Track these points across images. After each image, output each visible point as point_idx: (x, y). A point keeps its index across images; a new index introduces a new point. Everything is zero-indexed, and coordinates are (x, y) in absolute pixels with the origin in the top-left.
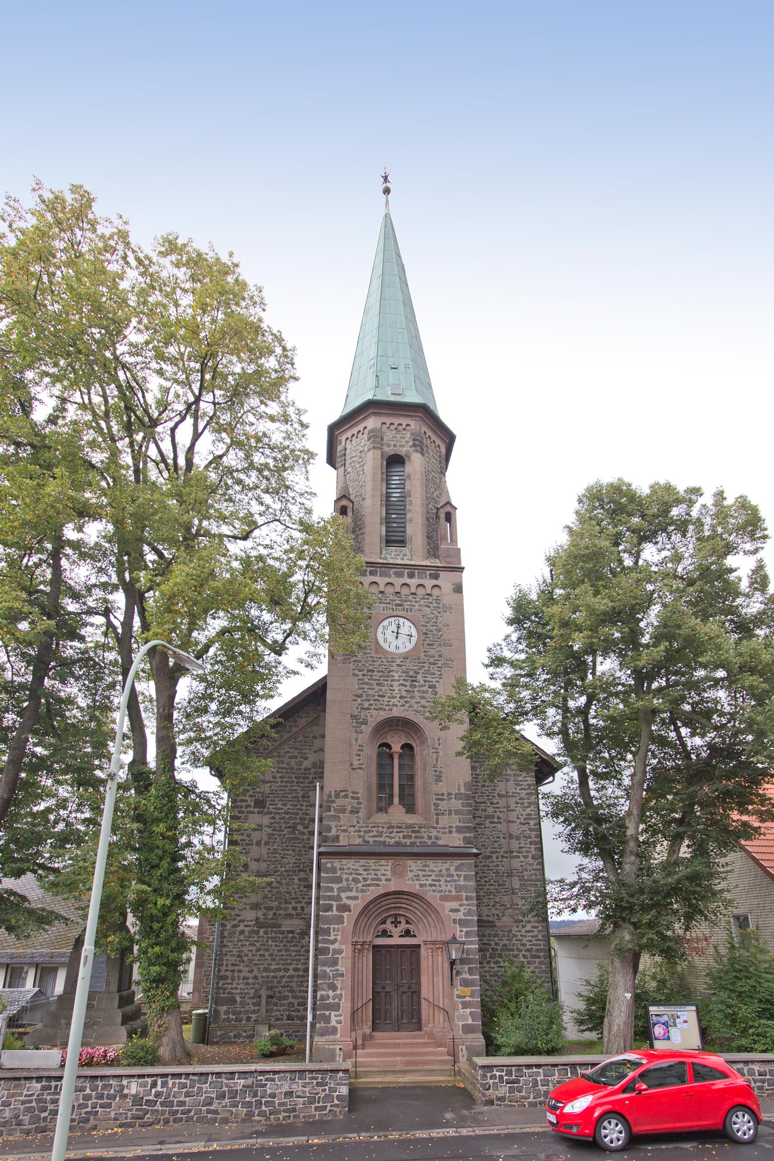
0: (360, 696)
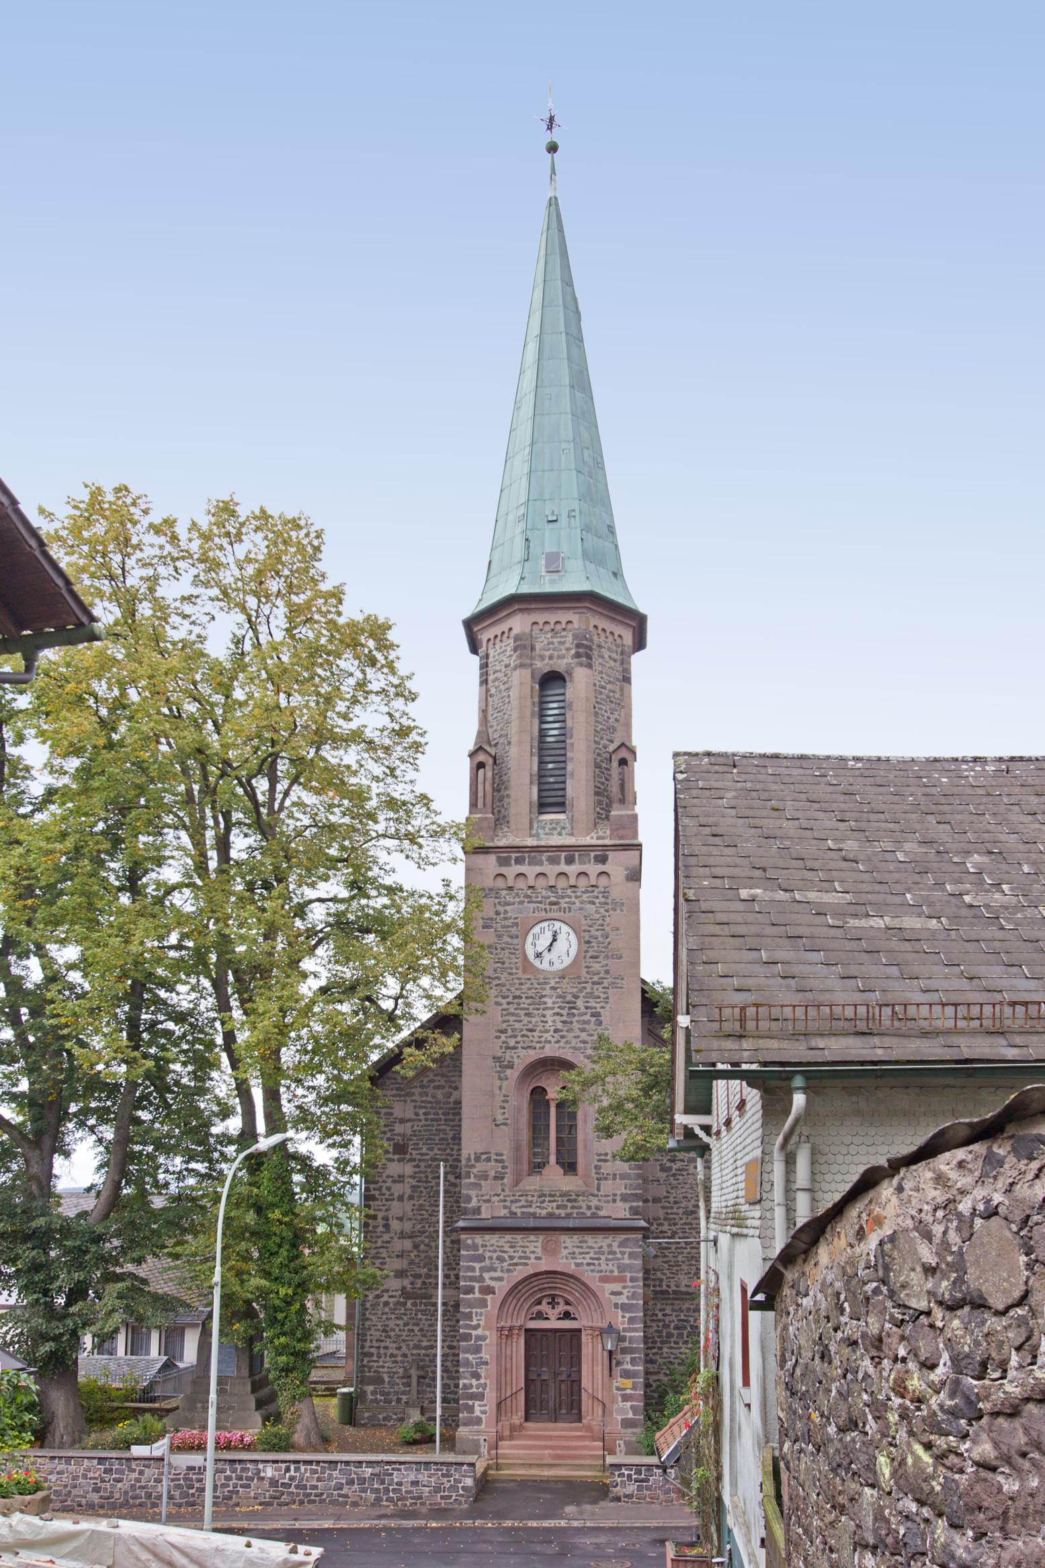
0: (504, 1031)
